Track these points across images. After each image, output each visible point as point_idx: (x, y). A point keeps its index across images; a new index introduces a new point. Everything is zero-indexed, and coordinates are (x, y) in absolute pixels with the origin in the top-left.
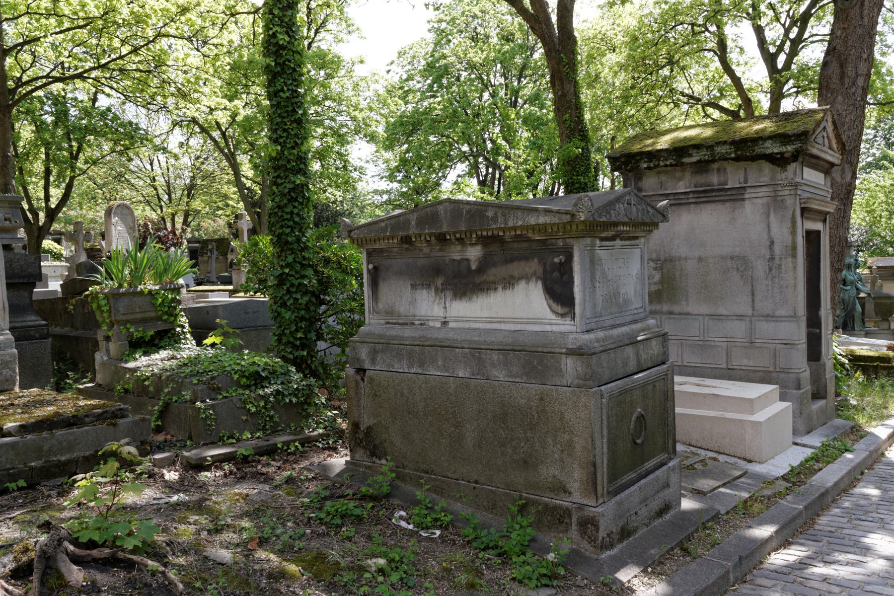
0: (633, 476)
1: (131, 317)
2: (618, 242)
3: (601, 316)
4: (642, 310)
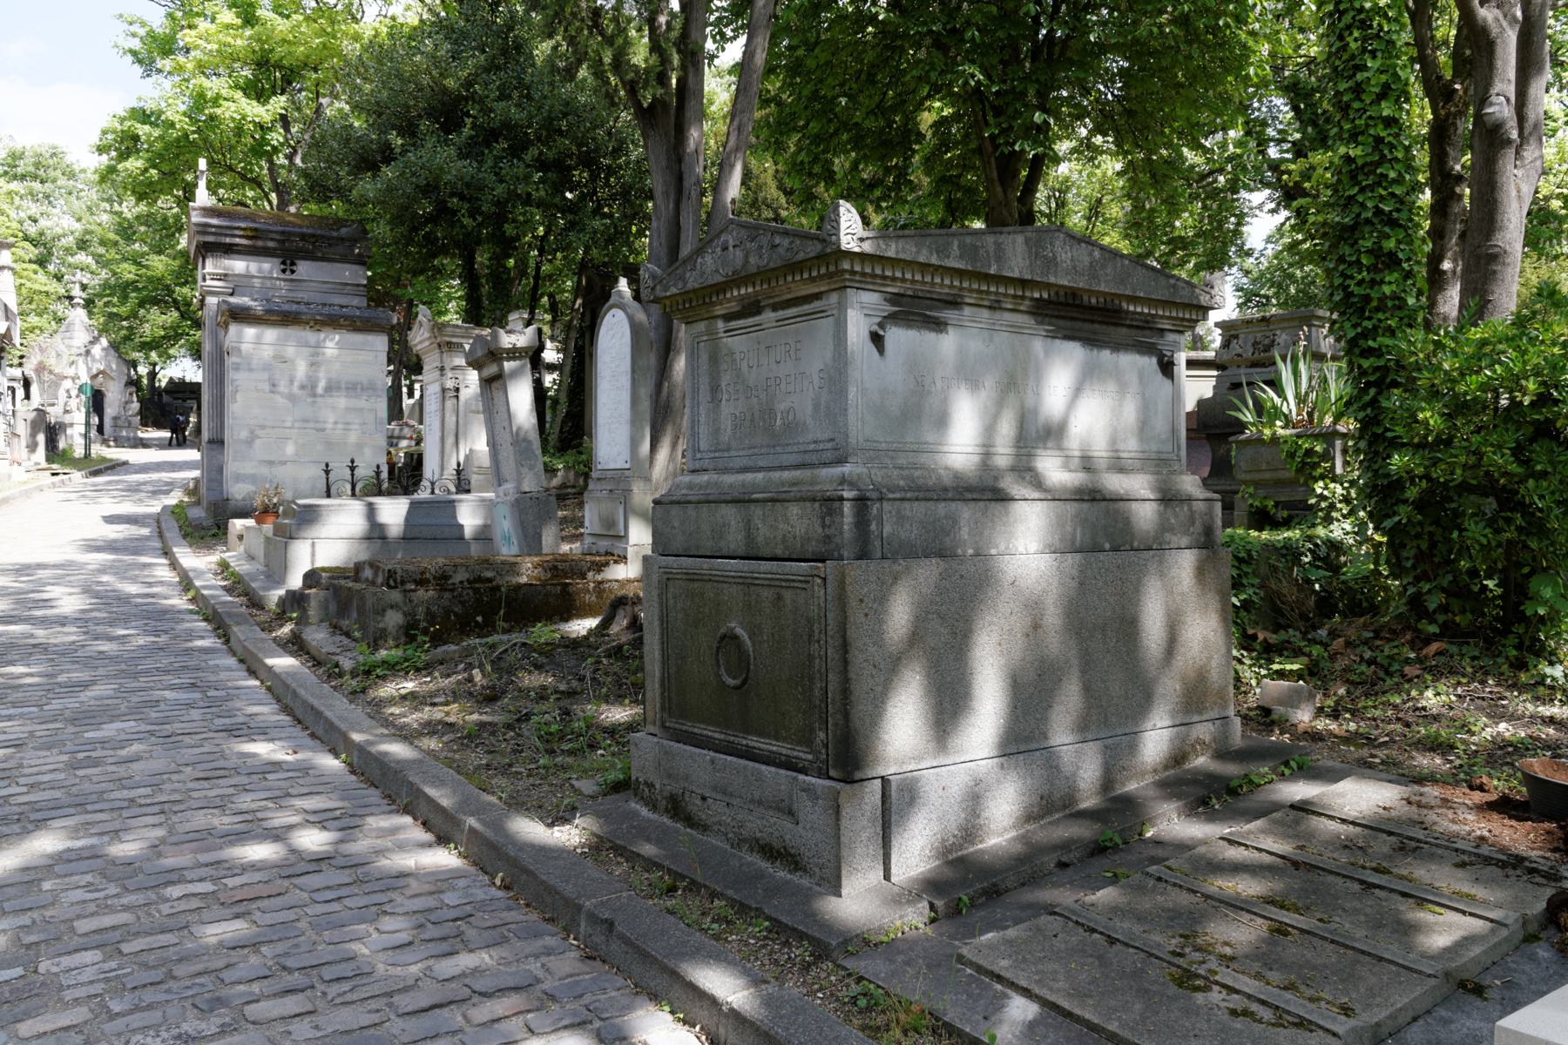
0: (717, 735)
1: (1257, 476)
2: (769, 316)
3: (728, 450)
4: (829, 445)
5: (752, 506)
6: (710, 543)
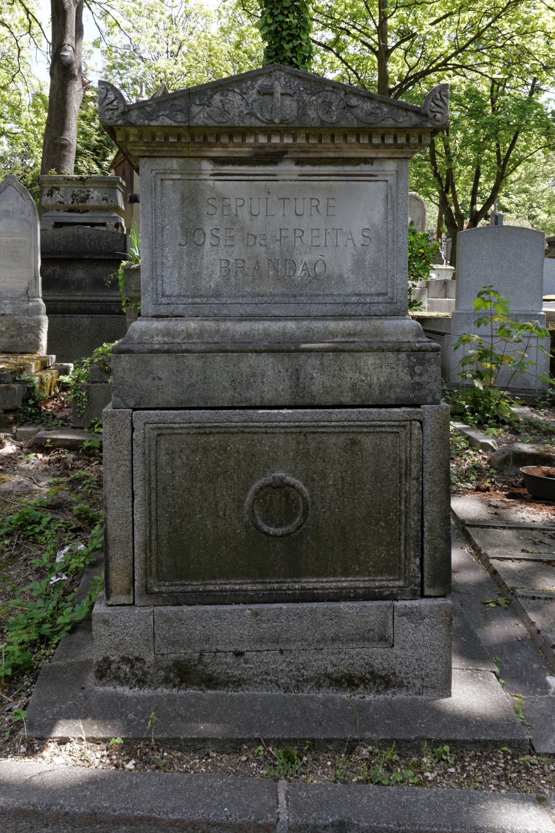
5: (303, 357)
6: (230, 393)
